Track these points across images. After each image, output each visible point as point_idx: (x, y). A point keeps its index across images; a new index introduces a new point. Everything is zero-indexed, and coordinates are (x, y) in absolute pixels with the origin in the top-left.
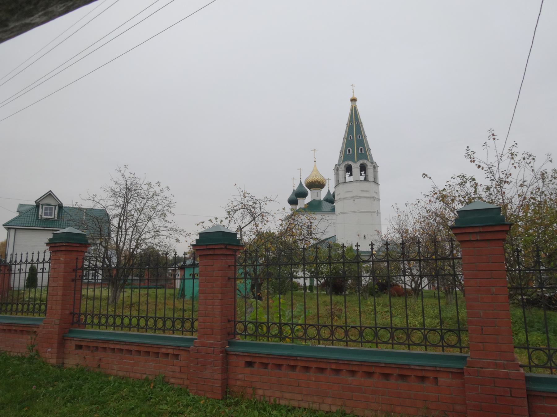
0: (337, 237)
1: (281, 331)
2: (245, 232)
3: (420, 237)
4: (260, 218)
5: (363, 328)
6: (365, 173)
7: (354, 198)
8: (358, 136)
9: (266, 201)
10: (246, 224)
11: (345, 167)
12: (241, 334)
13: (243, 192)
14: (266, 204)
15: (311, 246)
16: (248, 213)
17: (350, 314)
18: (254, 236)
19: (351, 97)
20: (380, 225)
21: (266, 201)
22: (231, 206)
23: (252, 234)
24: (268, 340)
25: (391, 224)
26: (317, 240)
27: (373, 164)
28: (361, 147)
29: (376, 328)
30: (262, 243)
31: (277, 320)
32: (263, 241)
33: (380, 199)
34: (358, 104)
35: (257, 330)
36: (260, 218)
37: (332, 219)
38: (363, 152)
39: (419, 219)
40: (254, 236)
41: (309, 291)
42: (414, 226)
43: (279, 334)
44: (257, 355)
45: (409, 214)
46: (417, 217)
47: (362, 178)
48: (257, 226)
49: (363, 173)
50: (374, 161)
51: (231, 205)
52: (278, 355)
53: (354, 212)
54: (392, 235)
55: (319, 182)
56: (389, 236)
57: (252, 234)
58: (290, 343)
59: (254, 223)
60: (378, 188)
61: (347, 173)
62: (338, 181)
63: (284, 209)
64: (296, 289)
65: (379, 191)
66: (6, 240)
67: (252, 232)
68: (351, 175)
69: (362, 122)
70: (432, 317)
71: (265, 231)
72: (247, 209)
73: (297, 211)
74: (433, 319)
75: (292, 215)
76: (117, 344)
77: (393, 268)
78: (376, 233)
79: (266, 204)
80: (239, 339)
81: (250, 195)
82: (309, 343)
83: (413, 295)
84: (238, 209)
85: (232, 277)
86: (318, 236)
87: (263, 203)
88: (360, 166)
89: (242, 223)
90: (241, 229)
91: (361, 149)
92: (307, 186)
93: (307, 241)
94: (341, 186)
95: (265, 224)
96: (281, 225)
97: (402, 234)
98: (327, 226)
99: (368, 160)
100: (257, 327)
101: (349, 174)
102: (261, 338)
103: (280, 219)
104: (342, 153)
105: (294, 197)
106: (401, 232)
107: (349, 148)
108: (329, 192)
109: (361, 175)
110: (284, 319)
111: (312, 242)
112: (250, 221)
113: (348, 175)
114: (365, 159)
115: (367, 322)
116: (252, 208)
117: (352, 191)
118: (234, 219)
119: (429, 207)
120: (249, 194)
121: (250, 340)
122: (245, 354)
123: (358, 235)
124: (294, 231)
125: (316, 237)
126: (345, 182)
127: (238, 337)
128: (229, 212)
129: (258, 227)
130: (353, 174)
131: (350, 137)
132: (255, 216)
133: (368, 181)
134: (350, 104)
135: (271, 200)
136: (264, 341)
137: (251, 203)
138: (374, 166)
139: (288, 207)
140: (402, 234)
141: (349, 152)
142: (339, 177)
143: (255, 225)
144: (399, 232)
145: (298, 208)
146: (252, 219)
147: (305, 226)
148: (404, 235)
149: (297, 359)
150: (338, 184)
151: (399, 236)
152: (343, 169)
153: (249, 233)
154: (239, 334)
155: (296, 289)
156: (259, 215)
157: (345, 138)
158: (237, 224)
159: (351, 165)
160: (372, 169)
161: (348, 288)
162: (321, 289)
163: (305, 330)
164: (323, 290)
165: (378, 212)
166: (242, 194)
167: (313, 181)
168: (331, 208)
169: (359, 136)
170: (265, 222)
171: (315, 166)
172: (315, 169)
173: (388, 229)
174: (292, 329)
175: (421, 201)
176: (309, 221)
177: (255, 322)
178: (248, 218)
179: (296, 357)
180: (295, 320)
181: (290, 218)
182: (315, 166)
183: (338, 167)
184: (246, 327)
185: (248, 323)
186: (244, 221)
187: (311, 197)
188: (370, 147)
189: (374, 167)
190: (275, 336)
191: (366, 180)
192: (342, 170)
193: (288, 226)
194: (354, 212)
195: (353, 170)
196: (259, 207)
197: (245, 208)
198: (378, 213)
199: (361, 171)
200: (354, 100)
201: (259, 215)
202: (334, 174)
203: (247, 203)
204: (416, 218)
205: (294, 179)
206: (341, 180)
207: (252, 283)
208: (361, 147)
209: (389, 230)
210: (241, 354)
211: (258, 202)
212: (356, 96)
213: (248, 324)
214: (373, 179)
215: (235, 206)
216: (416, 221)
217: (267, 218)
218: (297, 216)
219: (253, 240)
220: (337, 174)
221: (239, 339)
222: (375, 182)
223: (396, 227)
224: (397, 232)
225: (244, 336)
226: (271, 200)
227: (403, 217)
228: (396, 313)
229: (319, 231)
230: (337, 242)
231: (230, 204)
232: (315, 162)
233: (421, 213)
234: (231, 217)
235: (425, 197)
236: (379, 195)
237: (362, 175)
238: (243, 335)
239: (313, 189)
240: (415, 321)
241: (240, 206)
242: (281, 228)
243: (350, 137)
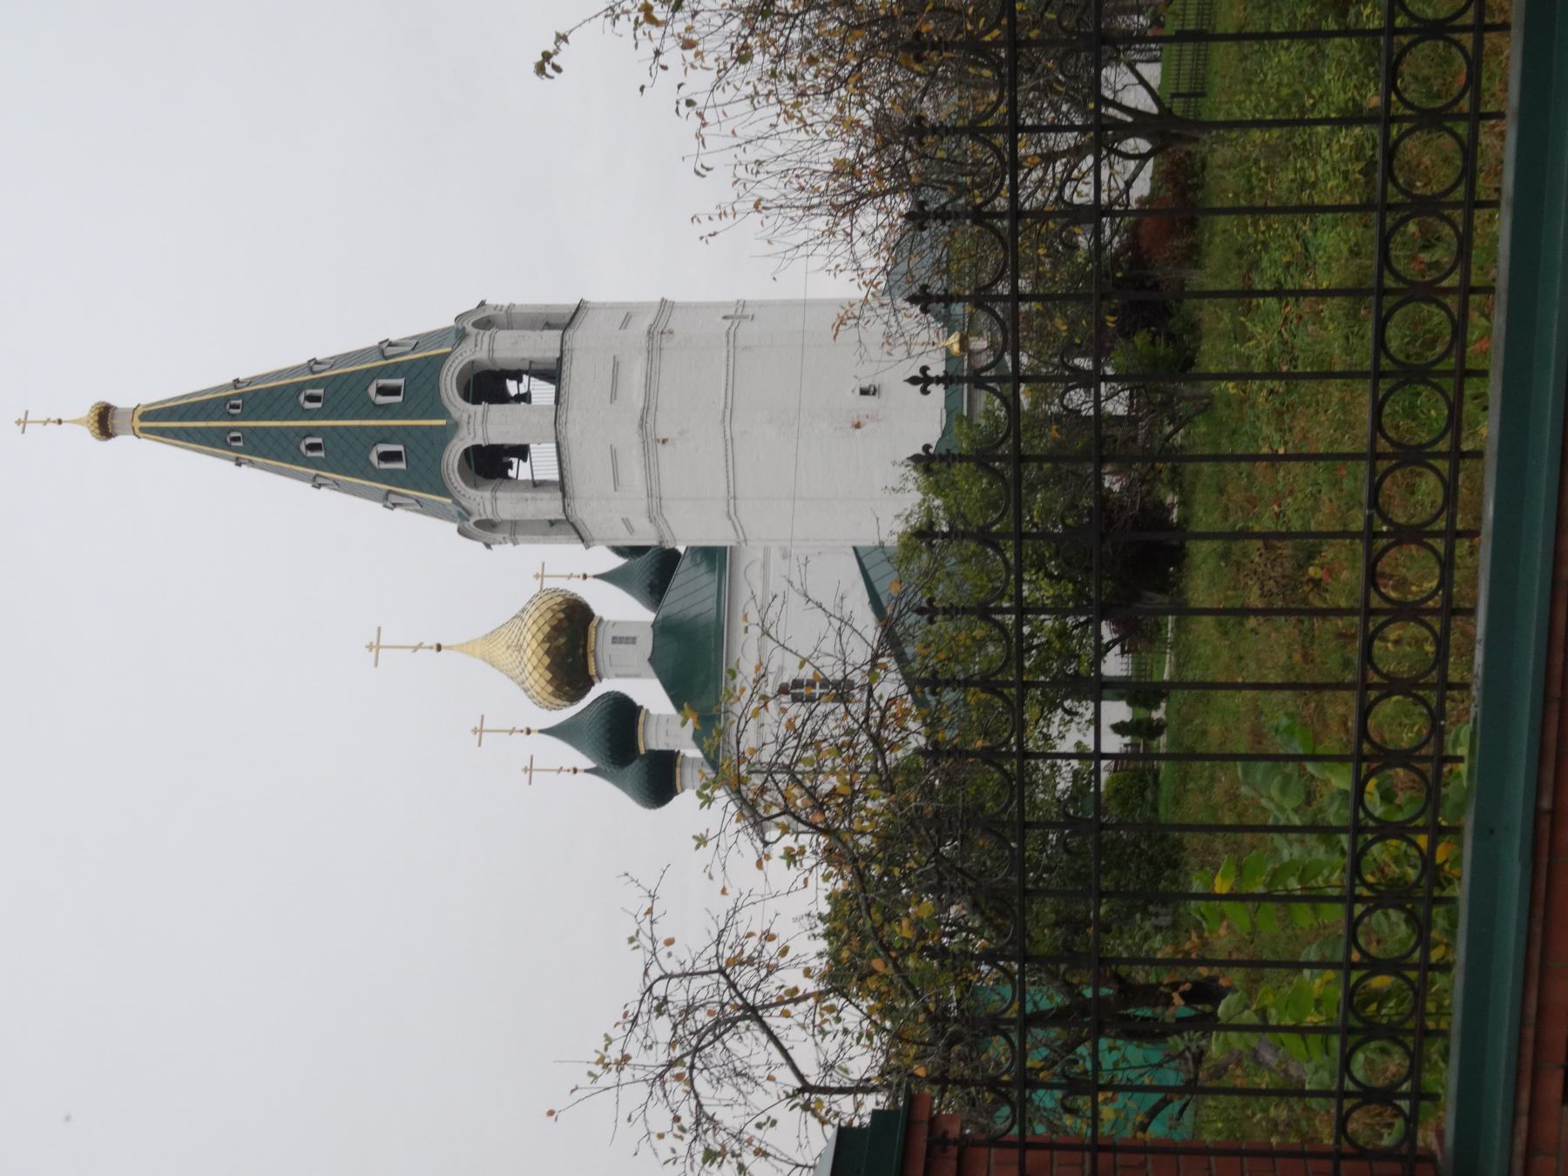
0: (868, 539)
1: (1392, 895)
2: (828, 1067)
3: (878, 98)
4: (746, 977)
5: (1383, 446)
6: (517, 376)
7: (651, 442)
8: (308, 405)
9: (653, 940)
10: (777, 1057)
11: (475, 486)
12: (1412, 1121)
13: (598, 1070)
14: (669, 942)
15: (911, 691)
16: (718, 1044)
17: (1291, 492)
18: (852, 1016)
19: (86, 436)
20: (805, 304)
21: (653, 940)
22: (677, 1144)
23: (840, 1027)
24: (1445, 967)
25: (803, 250)
26: (882, 660)
27: (469, 328)
28: (372, 390)
29: (1369, 612)
30: (890, 971)
31: (1334, 915)
32: (878, 964)
33: (664, 301)
34: (126, 398)
35: (1392, 1033)
36: (746, 977)
37: (765, 566)
38: (400, 382)
39: (780, 102)
40: (852, 1016)
41: (1163, 705)
42: (818, 128)
43: (1409, 906)
44: (1530, 1033)
45: (753, 153)
46: (770, 112)
47: (542, 392)
48: (794, 997)
49: (512, 387)
50: (450, 322)
51: (670, 1140)
52: (1531, 916)
53: (729, 443)
54: (862, 246)
55: (554, 628)
56: (869, 263)
57: (840, 1027)
58: (1460, 844)
59: (777, 1011)
60: (603, 306)
61: (512, 473)
62: (552, 523)
63: (701, 841)
64: (1150, 778)
65: (614, 307)
66: (567, 319)
67: (827, 1027)
68: (522, 452)
69: (229, 380)
70: (1312, 56)
71: (823, 945)
72: (697, 1049)
73: (713, 761)
74: (1324, 56)
75: (737, 794)
77: (1041, 251)
78: (849, 334)
79: (669, 942)
80: (1440, 1135)
81: (618, 1033)
82: (1460, 741)
83: (1191, 147)
84: (693, 1103)
85: (1087, 1167)
86: (860, 654)
87: (662, 955)
88: (476, 401)
89: (770, 1078)
90: (806, 1088)
91: (383, 391)
92: (574, 698)
93: (883, 717)
94: (583, 512)
95: (784, 951)
96: (791, 857)
97: (862, 196)
98: (803, 600)
99: (447, 355)
100: (1372, 1030)
101: (515, 460)
102: (1431, 1007)
103: (759, 864)
104: (393, 498)
105: (634, 770)
106: (849, 198)
107: (374, 458)
108: (610, 577)
109: (525, 398)
110: (1326, 872)
111: (890, 686)
112: (764, 1038)
113: (521, 470)
115: (1335, 400)
116: (690, 1024)
117: (614, 454)
118: (751, 1130)
119: (717, 46)
120: (609, 1040)
121: (1441, 1064)
122: (1524, 1103)
123: (858, 426)
124: (825, 788)
125: (867, 668)
126: (562, 485)
127: (1426, 1138)
128: (710, 1156)
129: (796, 990)
130: (517, 441)
131: (312, 447)
132: (738, 1008)
133: (560, 360)
134: (125, 443)
135: (650, 911)
136: (1452, 988)
137: (662, 1028)
138: (476, 325)
139: (685, 801)
140: (862, 196)
142: (528, 517)
143: (789, 1007)
144: (850, 209)
145: (692, 752)
146: (754, 1026)
147: (804, 724)
148: (865, 184)
149: (1553, 812)
150: (568, 527)
151: (870, 209)
152: (487, 494)
153: (831, 1046)
154: (1410, 1135)
155: (1150, 778)
156: (732, 985)
157: (315, 477)
158: (781, 1112)
159: (466, 451)
160: (492, 339)
161: (1149, 493)
162: (1151, 642)
163: (1388, 757)
164: (1159, 627)
165: (731, 312)
166: (609, 1079)
167: (547, 661)
168: (703, 568)
169: (311, 399)
170: (772, 948)
171: (462, 648)
172: (483, 648)
173: (832, 266)
174: (1385, 830)
175: (685, 93)
176: (771, 704)
177: (1344, 1043)
178: (747, 1045)
179: (1537, 811)
180: (1336, 814)
181: (752, 807)
182: (462, 648)
183: (473, 520)
184: (1368, 1095)
185: (1371, 673)
186: (759, 1072)
187: (637, 676)
188: (373, 341)
190: (1421, 927)
191: (552, 374)
193: (798, 819)
194: (729, 443)
195: (496, 439)
196: (685, 982)
197: (688, 1060)
198: (738, 314)
199: (502, 398)
200: (105, 421)
201: (732, 985)
202: (515, 543)
203: (662, 1047)
204: (774, 120)
205: (529, 770)
206: (549, 506)
207: (1117, 1037)
208: (372, 390)
209: (838, 260)
210: (1523, 1123)
211: (659, 990)
212: (84, 408)
213: (1353, 1079)
214: (548, 334)
215: (677, 1119)
216: (791, 117)
217: (750, 935)
218: (743, 768)
219: (873, 1023)
220: (515, 530)
221: (1440, 1135)
222: (565, 321)
223: (820, 223)
224: (845, 223)
225: (1424, 1104)
226: (650, 911)
227: (770, 189)
228: (1289, 247)
229: (829, 645)
230: (892, 541)
231: (664, 1147)
232: (439, 648)
233: (749, 90)
234: (736, 1147)
235: (664, 68)
236: (642, 307)
237: (523, 390)
238: (1415, 1108)
240: (1335, 147)
241: (678, 1090)
242: (809, 861)
243: (312, 447)
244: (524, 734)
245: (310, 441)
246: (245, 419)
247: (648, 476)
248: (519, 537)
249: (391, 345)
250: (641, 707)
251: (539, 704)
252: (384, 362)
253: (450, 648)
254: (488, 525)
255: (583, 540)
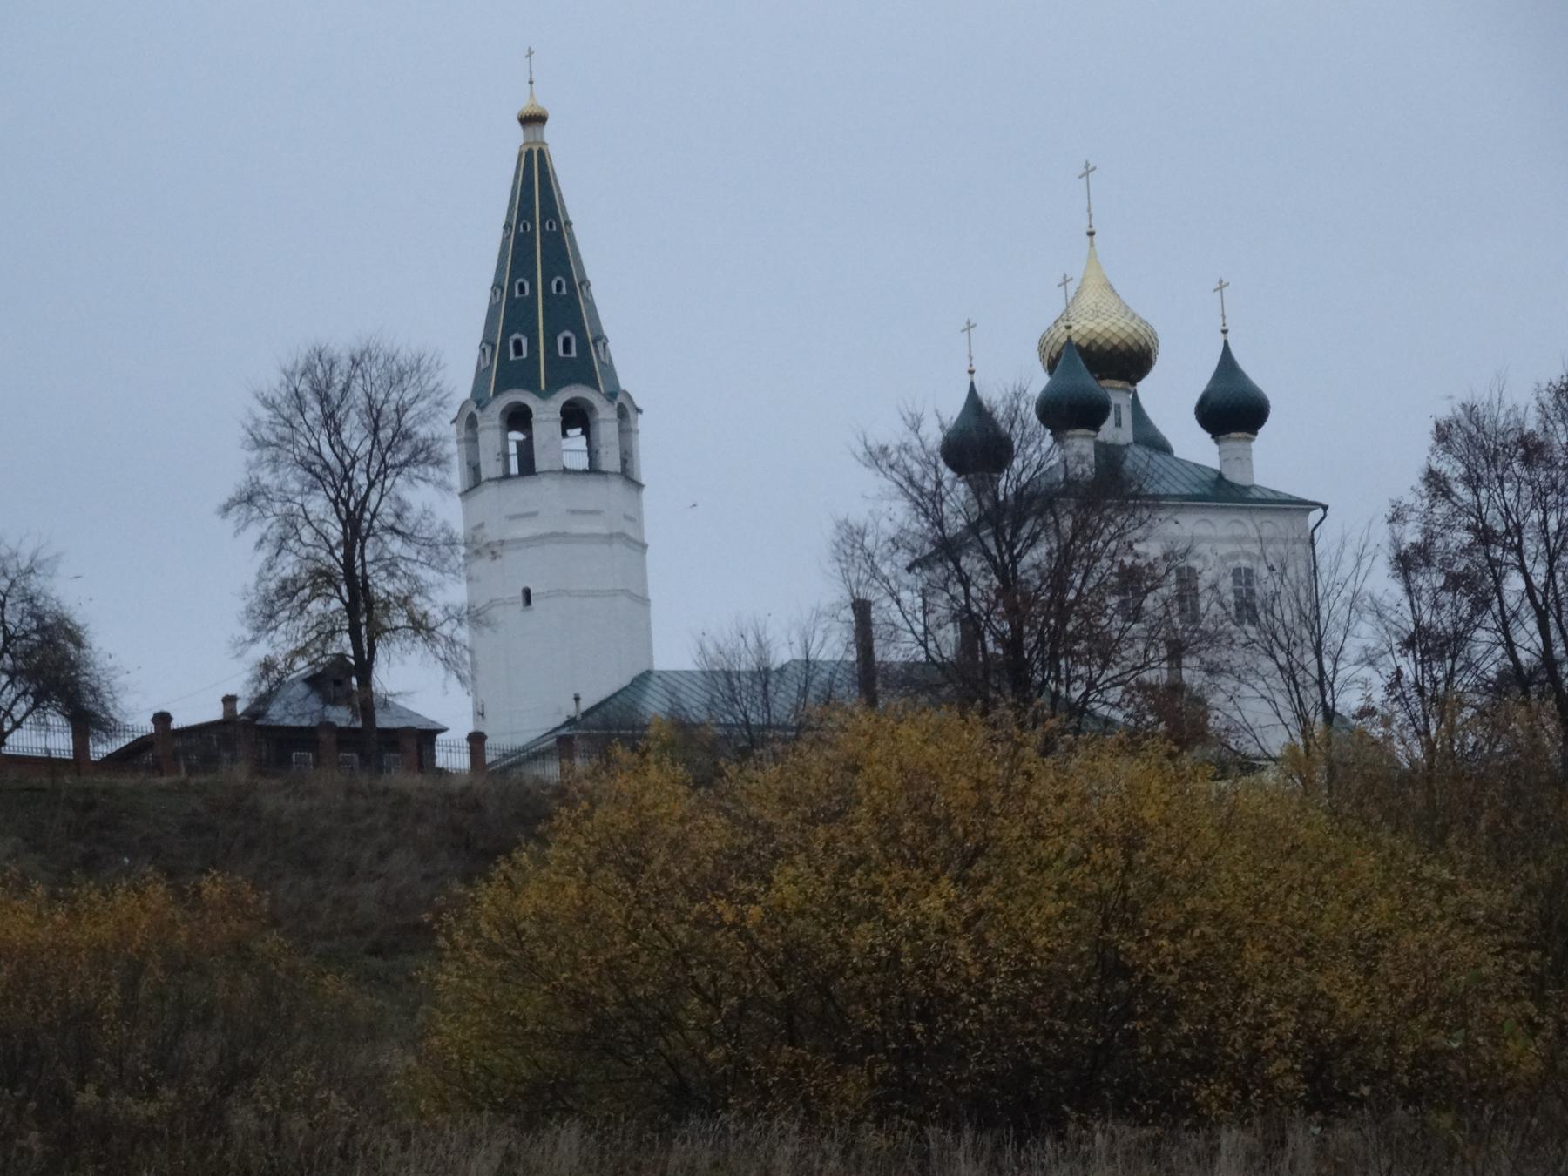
19: (523, 105)
28: (567, 334)
34: (551, 134)
50: (623, 386)
65: (640, 513)
66: (635, 478)
76: (1209, 507)
88: (563, 413)
91: (567, 342)
94: (488, 494)
99: (598, 389)
104: (489, 351)
114: (584, 383)
117: (534, 514)
134: (516, 137)
141: (518, 351)
160: (610, 421)
183: (478, 413)
188: (590, 276)
189: (622, 413)
191: (593, 469)
192: (494, 427)
200: (532, 120)
208: (567, 334)
212: (543, 103)
222: (627, 475)
239: (1240, 435)
244: (967, 368)
245: (527, 286)
246: (541, 235)
247: (525, 540)
248: (463, 445)
249: (605, 345)
250: (1255, 433)
251: (1043, 339)
252: (590, 337)
253: (1092, 244)
254: (472, 422)
255: (466, 492)
